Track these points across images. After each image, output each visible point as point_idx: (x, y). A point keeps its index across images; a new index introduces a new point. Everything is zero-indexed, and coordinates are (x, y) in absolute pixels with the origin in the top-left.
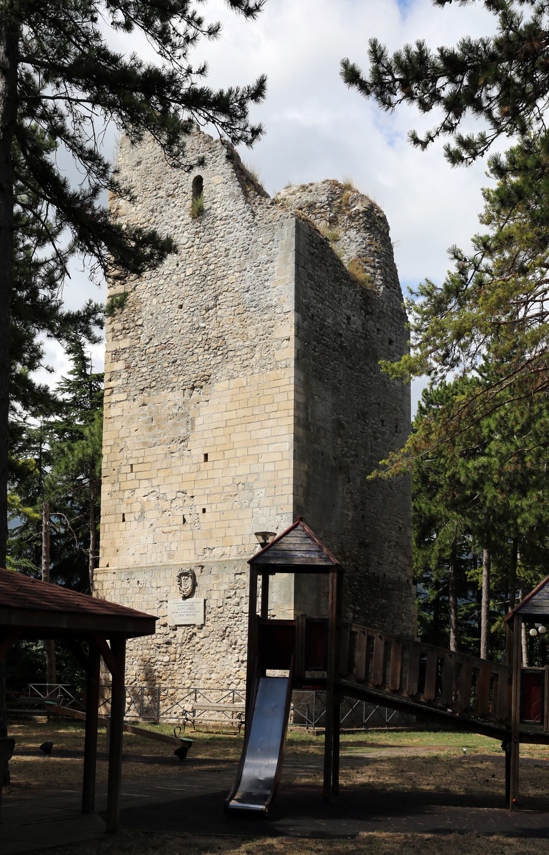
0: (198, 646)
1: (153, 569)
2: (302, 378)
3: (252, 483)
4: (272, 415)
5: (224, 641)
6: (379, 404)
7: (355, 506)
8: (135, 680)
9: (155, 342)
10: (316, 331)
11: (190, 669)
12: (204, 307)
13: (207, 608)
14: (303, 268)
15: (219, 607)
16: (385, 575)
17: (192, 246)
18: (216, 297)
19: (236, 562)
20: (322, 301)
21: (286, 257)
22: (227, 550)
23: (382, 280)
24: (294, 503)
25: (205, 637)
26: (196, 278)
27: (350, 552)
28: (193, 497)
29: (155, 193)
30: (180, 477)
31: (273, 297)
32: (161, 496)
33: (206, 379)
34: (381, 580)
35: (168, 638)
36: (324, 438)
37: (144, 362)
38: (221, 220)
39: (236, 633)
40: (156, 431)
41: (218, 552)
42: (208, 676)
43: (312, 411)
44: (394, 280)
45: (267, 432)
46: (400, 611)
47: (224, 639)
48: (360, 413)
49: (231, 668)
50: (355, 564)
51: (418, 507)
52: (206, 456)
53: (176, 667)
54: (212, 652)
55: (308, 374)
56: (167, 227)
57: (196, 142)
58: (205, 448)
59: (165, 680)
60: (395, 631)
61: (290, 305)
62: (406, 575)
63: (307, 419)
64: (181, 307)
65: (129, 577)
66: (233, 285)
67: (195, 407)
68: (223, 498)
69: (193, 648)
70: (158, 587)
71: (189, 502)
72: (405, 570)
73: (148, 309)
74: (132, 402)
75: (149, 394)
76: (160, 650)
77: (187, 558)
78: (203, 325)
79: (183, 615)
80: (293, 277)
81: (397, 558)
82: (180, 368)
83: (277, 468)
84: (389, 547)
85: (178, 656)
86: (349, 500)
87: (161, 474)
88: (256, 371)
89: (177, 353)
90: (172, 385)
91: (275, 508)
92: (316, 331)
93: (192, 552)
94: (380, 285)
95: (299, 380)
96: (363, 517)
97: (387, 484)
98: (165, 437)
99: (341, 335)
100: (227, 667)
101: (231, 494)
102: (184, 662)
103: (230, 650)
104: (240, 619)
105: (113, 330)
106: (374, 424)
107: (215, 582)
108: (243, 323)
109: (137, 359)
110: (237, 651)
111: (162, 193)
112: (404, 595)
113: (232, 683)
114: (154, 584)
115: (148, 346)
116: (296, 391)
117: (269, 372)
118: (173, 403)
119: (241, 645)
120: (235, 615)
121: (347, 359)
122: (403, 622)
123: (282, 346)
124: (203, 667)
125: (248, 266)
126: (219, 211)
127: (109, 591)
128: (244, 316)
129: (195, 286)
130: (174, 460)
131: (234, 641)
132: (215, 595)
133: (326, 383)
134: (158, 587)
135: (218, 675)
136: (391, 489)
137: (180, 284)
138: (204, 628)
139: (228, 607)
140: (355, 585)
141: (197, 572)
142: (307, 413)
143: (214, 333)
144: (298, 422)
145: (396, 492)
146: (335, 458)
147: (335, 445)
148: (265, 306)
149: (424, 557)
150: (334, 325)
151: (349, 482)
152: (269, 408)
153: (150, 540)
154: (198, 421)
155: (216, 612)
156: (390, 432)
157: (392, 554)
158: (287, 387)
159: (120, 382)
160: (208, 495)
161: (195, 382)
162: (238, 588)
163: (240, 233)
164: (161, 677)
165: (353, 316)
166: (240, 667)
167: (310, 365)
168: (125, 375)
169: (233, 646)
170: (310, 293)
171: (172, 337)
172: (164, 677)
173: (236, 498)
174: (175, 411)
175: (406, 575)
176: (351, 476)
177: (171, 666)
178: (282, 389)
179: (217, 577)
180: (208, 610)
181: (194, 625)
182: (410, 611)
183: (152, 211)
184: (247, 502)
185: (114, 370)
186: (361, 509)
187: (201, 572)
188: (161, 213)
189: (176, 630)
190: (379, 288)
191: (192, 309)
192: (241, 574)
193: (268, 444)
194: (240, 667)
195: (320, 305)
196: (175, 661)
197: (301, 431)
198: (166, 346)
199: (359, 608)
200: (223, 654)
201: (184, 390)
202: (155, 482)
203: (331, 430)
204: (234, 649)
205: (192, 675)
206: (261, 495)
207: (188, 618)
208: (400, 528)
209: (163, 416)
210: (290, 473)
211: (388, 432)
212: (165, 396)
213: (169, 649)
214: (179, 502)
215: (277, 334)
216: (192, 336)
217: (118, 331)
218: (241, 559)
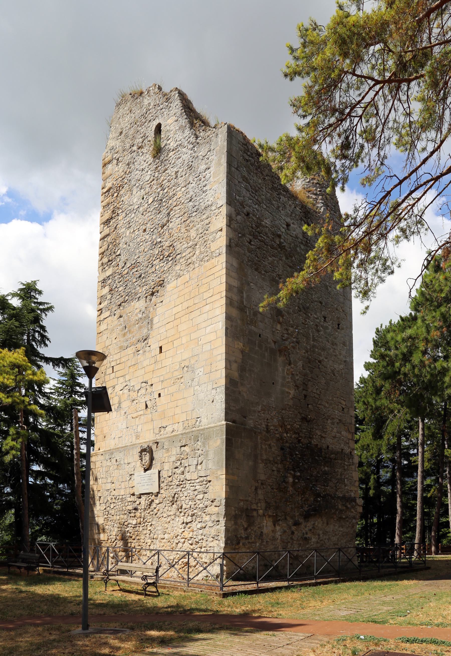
0: (155, 511)
1: (125, 448)
2: (235, 264)
3: (194, 364)
4: (209, 301)
5: (174, 506)
6: (321, 303)
7: (296, 386)
8: (116, 540)
9: (128, 265)
10: (252, 227)
11: (150, 530)
12: (160, 225)
13: (161, 478)
14: (237, 169)
15: (170, 477)
16: (328, 447)
17: (153, 180)
18: (169, 214)
19: (181, 436)
20: (259, 203)
21: (219, 160)
22: (175, 427)
23: (323, 203)
24: (226, 377)
25: (160, 503)
26: (155, 203)
27: (292, 425)
28: (152, 385)
29: (130, 150)
30: (143, 370)
31: (209, 198)
32: (131, 388)
33: (161, 284)
34: (323, 450)
35: (135, 505)
36: (261, 322)
37: (121, 283)
38: (173, 150)
39: (182, 499)
40: (129, 336)
41: (169, 429)
42: (162, 536)
43: (248, 296)
44: (334, 206)
45: (205, 316)
46: (343, 477)
47: (173, 504)
48: (301, 307)
49: (178, 530)
50: (297, 436)
51: (366, 401)
52: (161, 348)
53: (141, 529)
54: (165, 515)
55: (243, 262)
56: (138, 172)
57: (157, 99)
58: (160, 342)
59: (134, 539)
60: (337, 493)
61: (222, 200)
62: (349, 447)
63: (242, 302)
64: (145, 230)
65: (110, 457)
66: (181, 199)
67: (153, 309)
68: (172, 382)
69: (152, 513)
70: (129, 463)
71: (149, 390)
72: (348, 443)
73: (123, 240)
74: (113, 316)
75: (124, 307)
76: (130, 515)
77: (147, 438)
78: (159, 240)
79: (144, 485)
80: (225, 175)
81: (340, 433)
82: (143, 280)
83: (212, 347)
84: (333, 423)
85: (142, 520)
86: (290, 380)
87: (131, 370)
88: (197, 265)
89: (141, 269)
90: (138, 296)
91: (211, 383)
92: (252, 227)
93: (152, 431)
94: (321, 207)
95: (232, 265)
96: (305, 396)
97: (330, 371)
98: (134, 339)
99: (279, 236)
100: (175, 528)
101: (179, 377)
102: (146, 524)
103: (178, 513)
104: (185, 485)
105: (102, 264)
106: (317, 319)
107: (166, 455)
108: (188, 228)
109: (117, 282)
110: (182, 514)
111: (135, 148)
112: (346, 463)
113: (179, 542)
114: (126, 461)
115: (123, 269)
116: (227, 274)
117: (207, 264)
118: (139, 310)
119: (185, 509)
120: (181, 483)
121: (287, 258)
122: (345, 486)
123: (217, 237)
124: (159, 528)
125: (191, 179)
126: (172, 144)
127: (99, 469)
128: (188, 222)
129: (154, 211)
130: (139, 356)
131: (180, 505)
132: (166, 466)
133: (264, 274)
134: (129, 463)
135: (170, 535)
136: (334, 375)
137: (144, 213)
138: (159, 495)
139: (176, 476)
140: (296, 454)
141: (154, 448)
142: (242, 297)
143: (167, 244)
144: (230, 303)
145: (338, 378)
146: (275, 342)
147: (274, 330)
148: (203, 208)
149: (377, 445)
150: (272, 227)
151: (290, 364)
152: (206, 295)
153: (124, 426)
154: (155, 320)
155: (167, 481)
156: (333, 328)
157: (335, 430)
158: (220, 272)
159: (106, 303)
160: (162, 381)
161: (153, 288)
162: (183, 459)
163: (186, 155)
164: (131, 537)
165: (293, 223)
166: (185, 528)
167: (244, 254)
168: (109, 297)
169: (180, 510)
170: (244, 192)
171: (139, 257)
172: (133, 537)
173: (182, 380)
174: (140, 316)
175: (349, 447)
176: (291, 359)
177: (138, 528)
178: (217, 275)
179: (168, 450)
180: (162, 479)
181: (152, 493)
182: (352, 477)
183: (128, 164)
184: (190, 381)
185: (102, 295)
186: (303, 389)
187: (157, 447)
188: (134, 163)
189: (140, 498)
190: (320, 209)
191: (152, 230)
192: (185, 446)
193: (206, 327)
194: (185, 528)
195: (257, 206)
196: (140, 524)
197: (235, 313)
198: (133, 266)
199: (299, 474)
200: (173, 517)
201: (146, 297)
202: (127, 378)
203: (269, 316)
204: (181, 512)
205: (152, 535)
206: (201, 374)
207: (147, 487)
208: (343, 409)
209: (133, 322)
210: (223, 350)
211: (330, 327)
212: (134, 306)
213: (136, 514)
214: (143, 391)
215: (213, 228)
216: (152, 252)
217: (105, 264)
218: (185, 433)
